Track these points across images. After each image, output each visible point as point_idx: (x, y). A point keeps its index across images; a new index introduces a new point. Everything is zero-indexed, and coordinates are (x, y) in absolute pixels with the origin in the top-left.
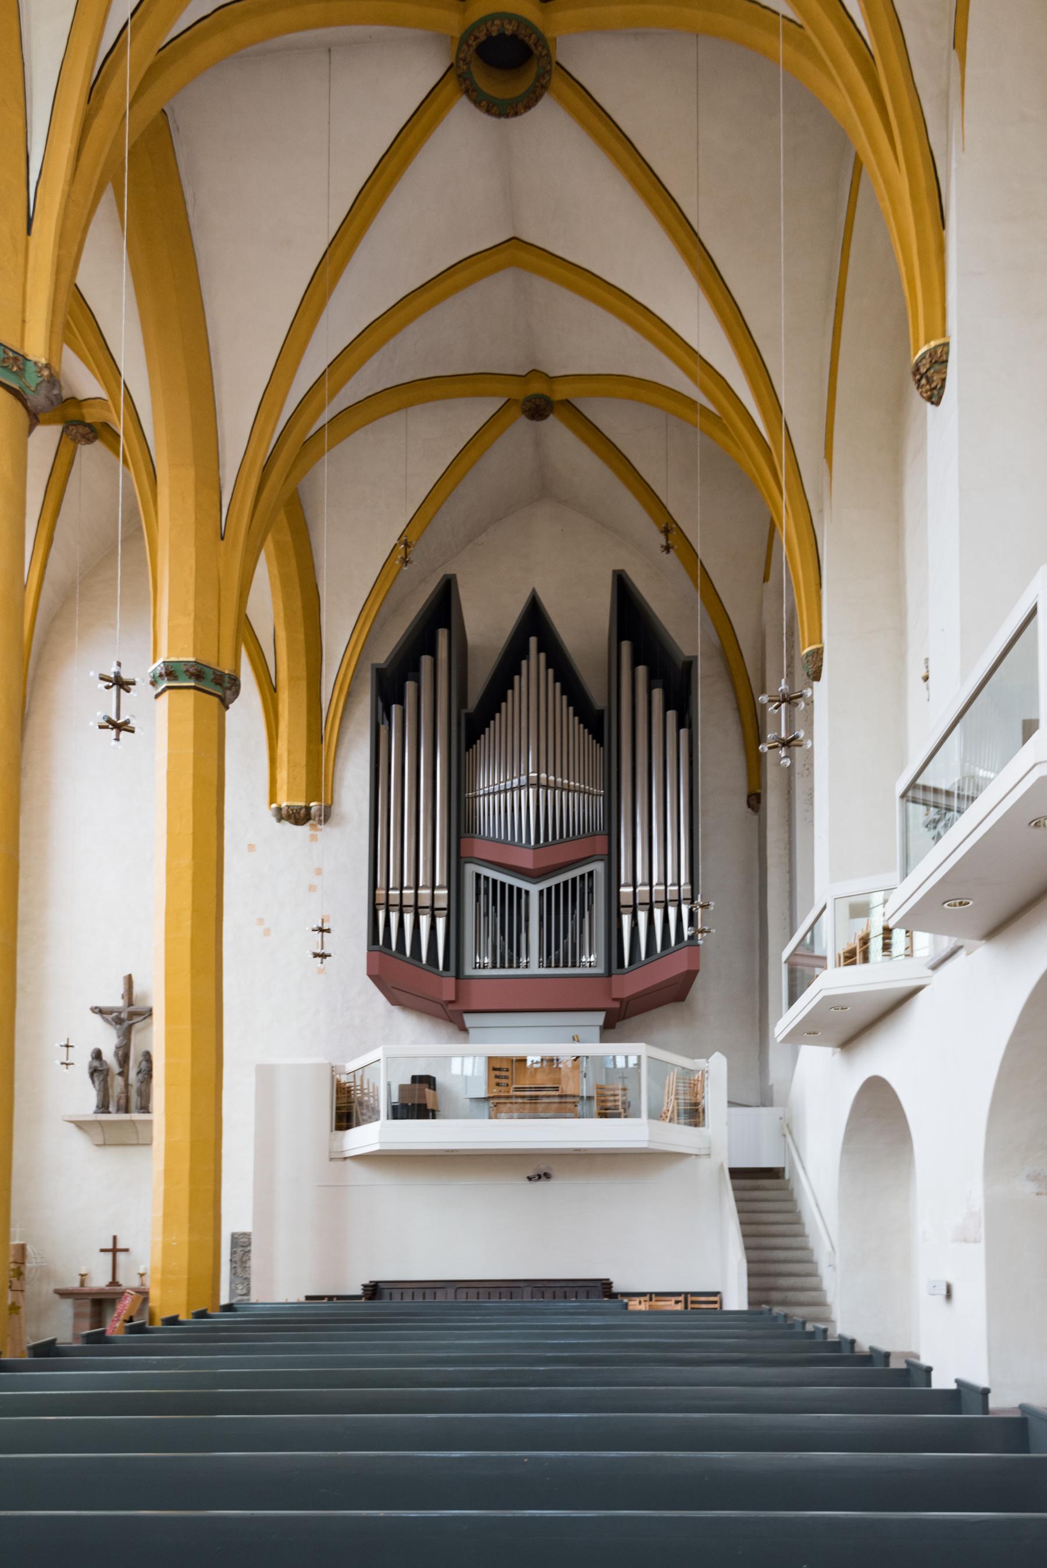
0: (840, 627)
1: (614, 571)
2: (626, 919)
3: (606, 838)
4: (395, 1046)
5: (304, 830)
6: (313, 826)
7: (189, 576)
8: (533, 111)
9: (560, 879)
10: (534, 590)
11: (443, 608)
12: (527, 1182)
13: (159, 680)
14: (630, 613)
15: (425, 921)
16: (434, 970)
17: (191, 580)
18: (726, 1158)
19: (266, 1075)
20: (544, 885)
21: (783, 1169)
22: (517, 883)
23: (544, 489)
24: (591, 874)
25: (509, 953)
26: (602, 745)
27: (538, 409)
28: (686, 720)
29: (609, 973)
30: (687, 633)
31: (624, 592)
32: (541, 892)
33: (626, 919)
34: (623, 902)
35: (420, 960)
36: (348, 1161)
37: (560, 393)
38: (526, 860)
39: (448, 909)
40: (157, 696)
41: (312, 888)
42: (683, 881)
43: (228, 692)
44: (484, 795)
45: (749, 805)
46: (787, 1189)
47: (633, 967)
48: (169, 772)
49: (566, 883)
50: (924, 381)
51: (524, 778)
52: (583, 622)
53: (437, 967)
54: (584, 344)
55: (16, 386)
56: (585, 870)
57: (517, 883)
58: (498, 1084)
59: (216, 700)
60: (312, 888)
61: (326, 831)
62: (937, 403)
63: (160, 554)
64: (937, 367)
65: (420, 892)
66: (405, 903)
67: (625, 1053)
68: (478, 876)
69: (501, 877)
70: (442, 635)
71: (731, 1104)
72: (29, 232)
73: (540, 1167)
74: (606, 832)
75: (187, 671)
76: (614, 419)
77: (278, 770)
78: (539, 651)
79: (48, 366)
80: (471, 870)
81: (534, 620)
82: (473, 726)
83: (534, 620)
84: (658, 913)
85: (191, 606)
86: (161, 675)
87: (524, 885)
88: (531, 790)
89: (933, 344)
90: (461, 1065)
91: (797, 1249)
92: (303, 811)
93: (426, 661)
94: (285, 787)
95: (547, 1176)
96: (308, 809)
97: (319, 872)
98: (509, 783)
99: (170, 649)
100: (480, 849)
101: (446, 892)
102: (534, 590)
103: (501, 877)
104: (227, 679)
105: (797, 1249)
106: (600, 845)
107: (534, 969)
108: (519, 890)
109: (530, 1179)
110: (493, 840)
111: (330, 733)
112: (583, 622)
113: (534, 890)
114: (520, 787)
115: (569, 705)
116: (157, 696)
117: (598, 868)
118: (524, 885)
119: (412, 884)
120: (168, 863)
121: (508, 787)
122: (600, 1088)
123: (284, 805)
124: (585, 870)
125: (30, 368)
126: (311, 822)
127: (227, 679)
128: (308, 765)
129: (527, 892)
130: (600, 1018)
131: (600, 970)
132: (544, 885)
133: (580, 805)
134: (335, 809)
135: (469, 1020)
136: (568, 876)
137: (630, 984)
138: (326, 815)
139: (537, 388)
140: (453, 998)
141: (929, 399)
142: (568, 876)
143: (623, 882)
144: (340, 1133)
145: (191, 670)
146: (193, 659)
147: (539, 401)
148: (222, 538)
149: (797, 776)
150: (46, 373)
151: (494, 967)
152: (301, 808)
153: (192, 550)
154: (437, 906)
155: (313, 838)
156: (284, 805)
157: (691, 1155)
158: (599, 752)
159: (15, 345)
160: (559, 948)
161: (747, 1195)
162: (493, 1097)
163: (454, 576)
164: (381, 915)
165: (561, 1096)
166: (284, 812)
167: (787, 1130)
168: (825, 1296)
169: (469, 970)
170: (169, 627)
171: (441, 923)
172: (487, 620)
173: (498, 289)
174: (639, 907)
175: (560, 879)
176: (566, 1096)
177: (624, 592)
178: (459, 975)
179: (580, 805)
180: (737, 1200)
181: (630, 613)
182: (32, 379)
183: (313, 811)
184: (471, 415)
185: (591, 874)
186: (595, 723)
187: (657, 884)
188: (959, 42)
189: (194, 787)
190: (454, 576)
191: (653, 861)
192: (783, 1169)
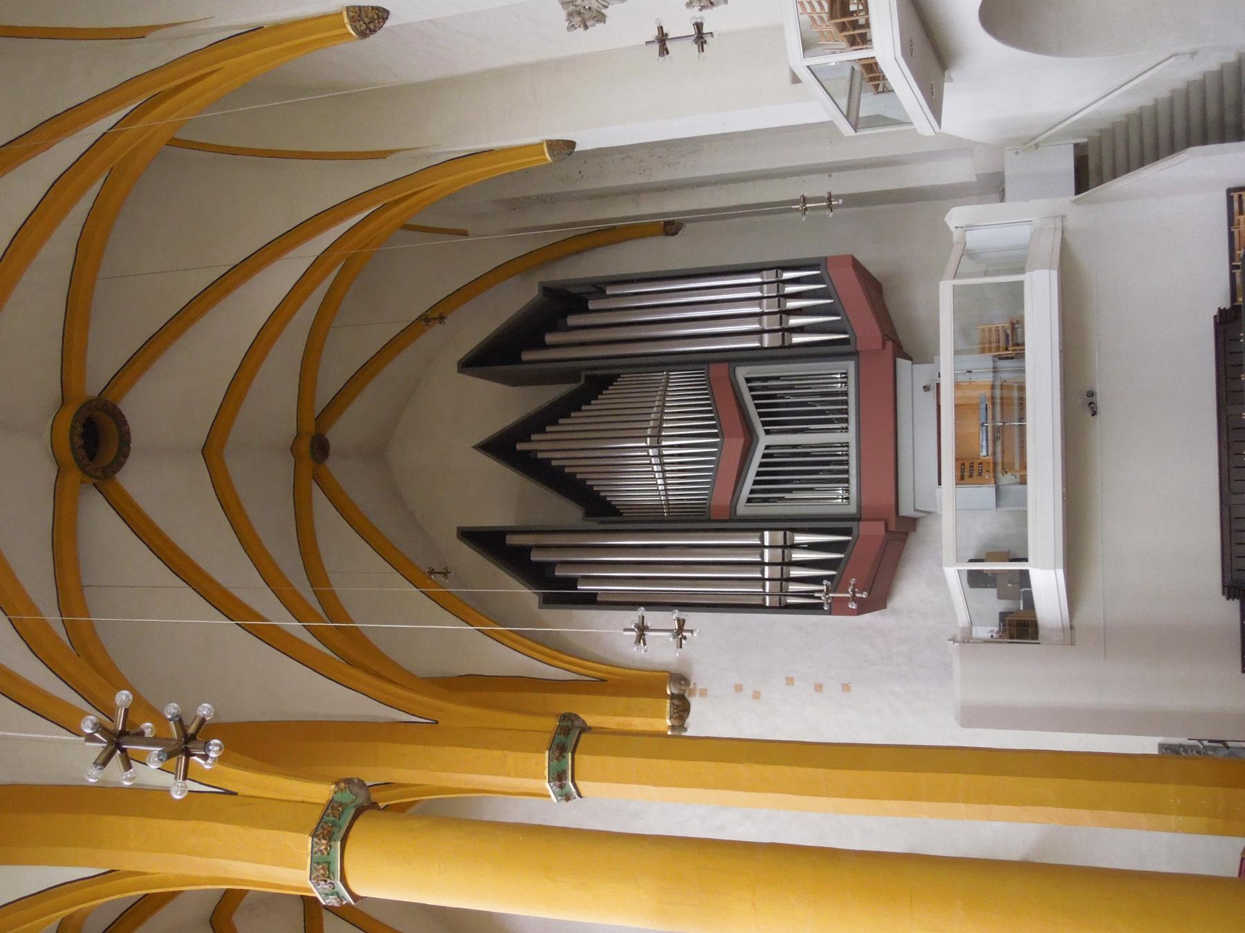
0: (523, 128)
1: (459, 371)
2: (797, 339)
3: (711, 366)
4: (937, 586)
5: (696, 704)
6: (692, 693)
7: (471, 754)
8: (129, 418)
9: (753, 412)
10: (475, 447)
11: (488, 541)
12: (1098, 416)
13: (565, 790)
14: (495, 358)
15: (797, 556)
16: (850, 545)
17: (475, 752)
18: (1065, 199)
19: (972, 716)
20: (760, 430)
21: (1076, 146)
22: (757, 459)
23: (377, 453)
24: (748, 380)
25: (828, 466)
26: (618, 376)
27: (320, 448)
28: (598, 288)
29: (853, 355)
30: (513, 300)
31: (476, 362)
32: (768, 432)
33: (797, 339)
34: (779, 343)
35: (839, 560)
36: (1075, 623)
37: (310, 427)
38: (737, 443)
39: (785, 530)
40: (580, 796)
41: (756, 695)
42: (758, 280)
43: (576, 723)
44: (667, 495)
45: (675, 233)
46: (1100, 138)
47: (849, 330)
48: (655, 784)
49: (758, 406)
50: (372, 26)
51: (651, 452)
52: (498, 404)
53: (848, 542)
54: (275, 405)
55: (352, 812)
56: (744, 387)
57: (757, 459)
58: (980, 474)
59: (584, 736)
60: (756, 695)
61: (699, 678)
62: (387, 12)
63: (450, 784)
64: (363, 14)
65: (766, 560)
66: (778, 576)
67: (943, 311)
68: (749, 500)
69: (751, 476)
70: (512, 540)
71: (1002, 199)
72: (235, 794)
73: (1080, 404)
74: (705, 366)
75: (557, 759)
76: (329, 383)
77: (633, 728)
78: (529, 441)
79: (337, 784)
80: (743, 509)
81: (501, 447)
82: (601, 510)
83: (501, 447)
84: (792, 304)
85: (498, 753)
86: (561, 787)
87: (760, 451)
88: (664, 443)
89: (346, 20)
90: (954, 516)
91: (1172, 122)
92: (676, 702)
93: (536, 557)
94: (651, 720)
95: (1091, 394)
96: (673, 697)
97: (739, 688)
98: (655, 468)
99: (535, 777)
100: (722, 498)
101: (767, 534)
102: (475, 447)
103: (751, 476)
104: (564, 723)
105: (1172, 122)
106: (718, 371)
107: (850, 437)
108: (764, 456)
109: (1094, 413)
110: (713, 484)
111: (599, 671)
112: (498, 404)
113: (764, 440)
114: (661, 456)
115: (580, 410)
116: (580, 796)
117: (742, 372)
118: (760, 451)
119: (759, 568)
120: (747, 790)
121: (659, 468)
122: (983, 351)
123: (669, 722)
124: (744, 387)
125: (338, 798)
126: (686, 695)
127: (564, 723)
128: (629, 696)
129: (767, 447)
130: (903, 364)
131: (850, 366)
132: (760, 430)
133: (679, 390)
134: (674, 668)
135: (906, 510)
136: (750, 404)
137: (867, 330)
138: (681, 679)
139: (305, 448)
140: (882, 524)
141: (385, 20)
142: (750, 404)
143: (757, 345)
144: (1041, 632)
145: (557, 754)
146: (547, 753)
147: (314, 447)
148: (437, 722)
149: (652, 180)
150: (342, 785)
151: (847, 481)
152: (672, 704)
153: (448, 749)
154: (782, 543)
155: (704, 693)
156: (669, 722)
157: (1063, 237)
158: (626, 378)
159: (318, 812)
160: (829, 411)
161: (1107, 167)
162: (995, 477)
163: (458, 528)
164: (791, 600)
165: (993, 404)
166: (676, 723)
167: (1030, 143)
168: (1229, 65)
169: (852, 509)
170: (517, 776)
171: (800, 538)
172: (500, 497)
173: (236, 467)
174: (784, 326)
175: (753, 412)
176: (993, 398)
177: (476, 362)
178: (856, 518)
179: (679, 390)
180: (1114, 177)
181: (495, 358)
182: (347, 797)
183: (675, 692)
184: (324, 512)
185: (748, 380)
186: (596, 383)
187: (761, 306)
188: (138, 33)
189: (670, 758)
190: (458, 528)
191: (733, 313)
192: (1076, 146)
